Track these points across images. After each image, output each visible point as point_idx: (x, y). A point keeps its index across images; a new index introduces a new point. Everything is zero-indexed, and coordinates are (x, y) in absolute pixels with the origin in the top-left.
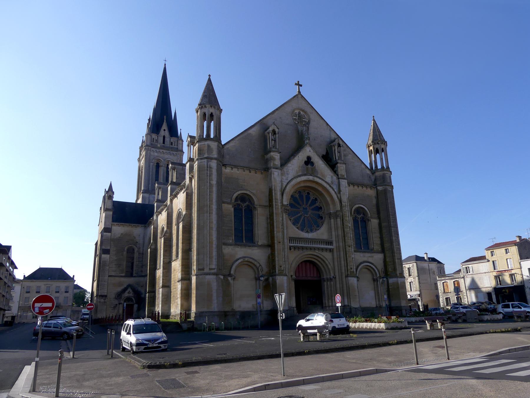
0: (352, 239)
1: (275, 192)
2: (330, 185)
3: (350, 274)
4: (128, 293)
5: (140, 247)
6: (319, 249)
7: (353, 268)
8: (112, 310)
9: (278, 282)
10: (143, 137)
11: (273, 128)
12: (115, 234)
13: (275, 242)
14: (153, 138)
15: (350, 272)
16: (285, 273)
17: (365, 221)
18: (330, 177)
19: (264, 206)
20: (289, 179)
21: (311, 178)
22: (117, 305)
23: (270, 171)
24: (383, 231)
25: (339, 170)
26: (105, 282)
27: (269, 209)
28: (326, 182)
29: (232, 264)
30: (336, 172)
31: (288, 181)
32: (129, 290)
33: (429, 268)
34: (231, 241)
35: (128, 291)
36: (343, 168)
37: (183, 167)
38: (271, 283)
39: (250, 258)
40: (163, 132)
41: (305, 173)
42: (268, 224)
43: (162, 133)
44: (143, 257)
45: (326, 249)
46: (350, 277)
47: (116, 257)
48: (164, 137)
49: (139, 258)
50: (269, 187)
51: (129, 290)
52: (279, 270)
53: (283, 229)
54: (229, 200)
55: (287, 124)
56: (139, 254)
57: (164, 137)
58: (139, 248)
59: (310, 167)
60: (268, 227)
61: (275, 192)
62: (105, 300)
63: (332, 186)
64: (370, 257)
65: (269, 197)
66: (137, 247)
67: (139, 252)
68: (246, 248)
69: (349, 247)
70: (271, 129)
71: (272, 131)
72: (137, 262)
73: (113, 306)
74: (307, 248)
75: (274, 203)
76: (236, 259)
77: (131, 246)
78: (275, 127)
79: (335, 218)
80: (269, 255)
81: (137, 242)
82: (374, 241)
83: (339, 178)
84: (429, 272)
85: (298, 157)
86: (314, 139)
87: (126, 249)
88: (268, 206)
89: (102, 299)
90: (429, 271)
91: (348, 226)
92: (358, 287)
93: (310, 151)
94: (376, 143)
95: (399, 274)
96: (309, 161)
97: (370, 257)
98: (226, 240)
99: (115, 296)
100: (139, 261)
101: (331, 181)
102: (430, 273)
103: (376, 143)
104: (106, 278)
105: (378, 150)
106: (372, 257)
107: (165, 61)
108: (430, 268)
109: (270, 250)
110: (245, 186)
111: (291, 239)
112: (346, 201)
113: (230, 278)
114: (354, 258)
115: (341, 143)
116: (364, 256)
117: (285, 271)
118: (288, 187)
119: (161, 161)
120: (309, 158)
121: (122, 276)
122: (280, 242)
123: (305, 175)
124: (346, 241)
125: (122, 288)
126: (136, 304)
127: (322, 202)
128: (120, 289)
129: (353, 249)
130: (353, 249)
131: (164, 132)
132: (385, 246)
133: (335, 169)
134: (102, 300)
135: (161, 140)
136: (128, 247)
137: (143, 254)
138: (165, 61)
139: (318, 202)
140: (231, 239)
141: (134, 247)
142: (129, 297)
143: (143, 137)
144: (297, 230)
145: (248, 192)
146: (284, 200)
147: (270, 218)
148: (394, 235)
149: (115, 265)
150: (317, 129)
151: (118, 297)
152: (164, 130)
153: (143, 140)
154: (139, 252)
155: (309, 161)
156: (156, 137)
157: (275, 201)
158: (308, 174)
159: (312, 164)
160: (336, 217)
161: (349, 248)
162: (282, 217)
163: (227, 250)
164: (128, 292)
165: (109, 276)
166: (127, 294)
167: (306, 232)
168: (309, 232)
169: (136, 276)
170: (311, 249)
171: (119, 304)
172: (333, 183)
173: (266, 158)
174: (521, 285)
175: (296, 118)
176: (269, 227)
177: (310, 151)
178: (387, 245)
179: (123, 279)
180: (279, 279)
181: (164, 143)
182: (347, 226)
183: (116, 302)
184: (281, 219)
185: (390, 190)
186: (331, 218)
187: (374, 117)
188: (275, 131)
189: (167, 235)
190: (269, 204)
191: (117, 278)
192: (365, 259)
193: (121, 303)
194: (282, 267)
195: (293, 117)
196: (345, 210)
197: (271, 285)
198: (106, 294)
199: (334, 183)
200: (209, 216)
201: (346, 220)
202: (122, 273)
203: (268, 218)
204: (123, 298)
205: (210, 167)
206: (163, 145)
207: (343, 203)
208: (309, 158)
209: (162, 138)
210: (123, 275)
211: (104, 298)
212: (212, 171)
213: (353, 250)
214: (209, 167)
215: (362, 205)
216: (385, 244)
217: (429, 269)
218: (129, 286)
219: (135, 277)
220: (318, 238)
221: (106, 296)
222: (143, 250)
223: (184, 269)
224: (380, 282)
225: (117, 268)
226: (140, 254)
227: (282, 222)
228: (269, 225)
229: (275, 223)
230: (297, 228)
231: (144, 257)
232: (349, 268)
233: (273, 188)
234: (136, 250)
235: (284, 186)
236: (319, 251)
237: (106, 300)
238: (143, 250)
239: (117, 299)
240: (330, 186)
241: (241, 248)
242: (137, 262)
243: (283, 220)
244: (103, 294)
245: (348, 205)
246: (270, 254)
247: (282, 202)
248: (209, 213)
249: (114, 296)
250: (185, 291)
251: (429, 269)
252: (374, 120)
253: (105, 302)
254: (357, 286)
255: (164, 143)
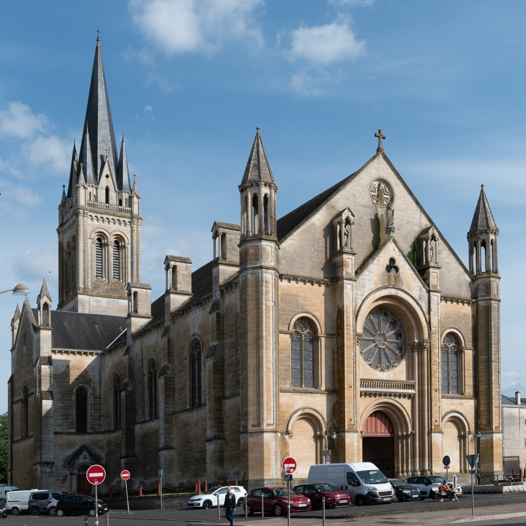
0: (440, 381)
1: (347, 315)
2: (418, 301)
3: (434, 428)
4: (83, 458)
5: (95, 386)
6: (395, 395)
7: (438, 421)
8: (61, 483)
9: (347, 440)
10: (64, 186)
11: (347, 215)
12: (57, 366)
13: (345, 386)
14: (90, 193)
15: (434, 426)
16: (356, 428)
17: (459, 352)
18: (418, 289)
19: (331, 335)
20: (366, 295)
21: (393, 292)
22: (67, 476)
23: (340, 283)
24: (480, 367)
25: (431, 279)
26: (49, 441)
27: (337, 339)
28: (413, 298)
29: (289, 417)
30: (426, 280)
31: (364, 298)
32: (85, 453)
33: (519, 415)
34: (288, 386)
35: (82, 456)
36: (436, 274)
37: (187, 265)
38: (336, 442)
39: (312, 409)
40: (106, 181)
41: (386, 285)
42: (333, 360)
43: (104, 182)
44: (100, 402)
45: (405, 396)
46: (434, 432)
47: (62, 403)
48: (107, 190)
49: (94, 404)
50: (338, 306)
51: (85, 453)
52: (349, 425)
53: (356, 368)
54: (285, 328)
55: (363, 206)
56: (94, 398)
57: (107, 190)
58: (94, 389)
59: (392, 274)
60: (334, 364)
61: (347, 315)
62: (52, 469)
63: (420, 303)
64: (459, 404)
65: (337, 322)
66: (90, 387)
67: (94, 395)
68: (306, 395)
69: (436, 391)
70: (344, 216)
71: (345, 219)
72: (92, 410)
73: (61, 478)
74: (380, 394)
75: (345, 331)
76: (294, 410)
77: (82, 385)
78: (350, 213)
79: (420, 350)
80: (334, 404)
81: (90, 380)
82: (467, 382)
83: (429, 292)
84: (518, 421)
85: (378, 259)
86: (398, 228)
87: (74, 391)
88: (334, 335)
89: (47, 467)
90: (520, 419)
91: (437, 362)
92: (442, 446)
93: (394, 250)
94: (484, 232)
95: (495, 429)
96: (392, 266)
97: (459, 404)
98: (283, 385)
99: (64, 463)
100: (94, 409)
101: (419, 296)
102: (520, 423)
103: (484, 232)
104: (52, 436)
105: (485, 242)
106: (462, 404)
107: (98, 31)
108: (521, 416)
109: (336, 398)
110: (305, 305)
111: (365, 382)
112: (437, 325)
113: (287, 436)
114: (440, 407)
115: (437, 234)
116: (452, 404)
117: (355, 425)
118: (363, 308)
119: (104, 235)
120: (392, 260)
121: (71, 434)
122: (351, 387)
123: (386, 287)
124: (433, 382)
125: (74, 450)
126: (473, 453)
127: (403, 326)
128: (70, 452)
129: (440, 394)
130: (440, 394)
131: (107, 180)
132: (480, 389)
133: (425, 276)
134: (48, 470)
135: (102, 197)
136: (77, 387)
137: (100, 398)
138: (98, 31)
139: (397, 326)
140: (288, 383)
141: (87, 386)
142: (85, 464)
143: (64, 186)
144: (369, 367)
145: (310, 316)
146: (358, 326)
147: (337, 352)
148: (495, 373)
149: (61, 415)
150: (403, 211)
151: (68, 464)
152: (107, 176)
153: (64, 193)
154: (94, 395)
155: (392, 266)
156: (95, 190)
157: (347, 328)
158: (390, 286)
159: (397, 269)
160: (421, 349)
161: (436, 393)
162: (354, 351)
163: (284, 398)
164: (83, 456)
165: (55, 433)
166: (82, 460)
167: (380, 371)
168: (384, 371)
169: (92, 433)
170: (385, 395)
171: (72, 474)
172: (421, 298)
173: (333, 263)
174: (480, 444)
175: (375, 193)
176: (336, 365)
177: (394, 250)
178: (483, 388)
179: (73, 438)
180: (348, 436)
181: (107, 201)
182: (435, 361)
183: (68, 472)
184: (353, 354)
185: (495, 307)
186: (414, 350)
187: (482, 186)
188: (350, 220)
189: (169, 372)
190: (338, 331)
191: (65, 437)
192: (453, 408)
193: (75, 474)
194: (353, 420)
195: (371, 193)
196: (434, 339)
197: (336, 445)
198: (52, 460)
199: (423, 298)
200: (266, 353)
201: (435, 353)
202: (71, 428)
203: (333, 352)
204: (76, 465)
205: (266, 281)
206: (107, 205)
207: (432, 328)
208: (392, 260)
209: (104, 192)
210: (74, 430)
211: (50, 466)
212: (268, 287)
213: (440, 396)
214: (264, 282)
215: (456, 329)
216: (480, 386)
217: (519, 416)
218: (83, 448)
219: (90, 433)
220: (395, 379)
221: (52, 463)
222: (100, 392)
223: (217, 424)
224: (468, 439)
225: (63, 421)
226: (97, 397)
227: (354, 358)
228: (336, 362)
229: (346, 360)
230: (370, 365)
231: (101, 403)
232: (433, 420)
233: (345, 309)
234: (90, 392)
235: (359, 305)
236: (395, 398)
237: (53, 470)
238: (100, 392)
239: (67, 467)
240: (418, 303)
241: (301, 395)
242: (93, 411)
243: (355, 356)
244: (48, 460)
245: (439, 331)
246: (336, 402)
247: (355, 330)
248: (266, 349)
249: (62, 463)
250: (219, 454)
251: (519, 416)
252: (482, 191)
253: (52, 472)
254: (441, 444)
255: (107, 201)
